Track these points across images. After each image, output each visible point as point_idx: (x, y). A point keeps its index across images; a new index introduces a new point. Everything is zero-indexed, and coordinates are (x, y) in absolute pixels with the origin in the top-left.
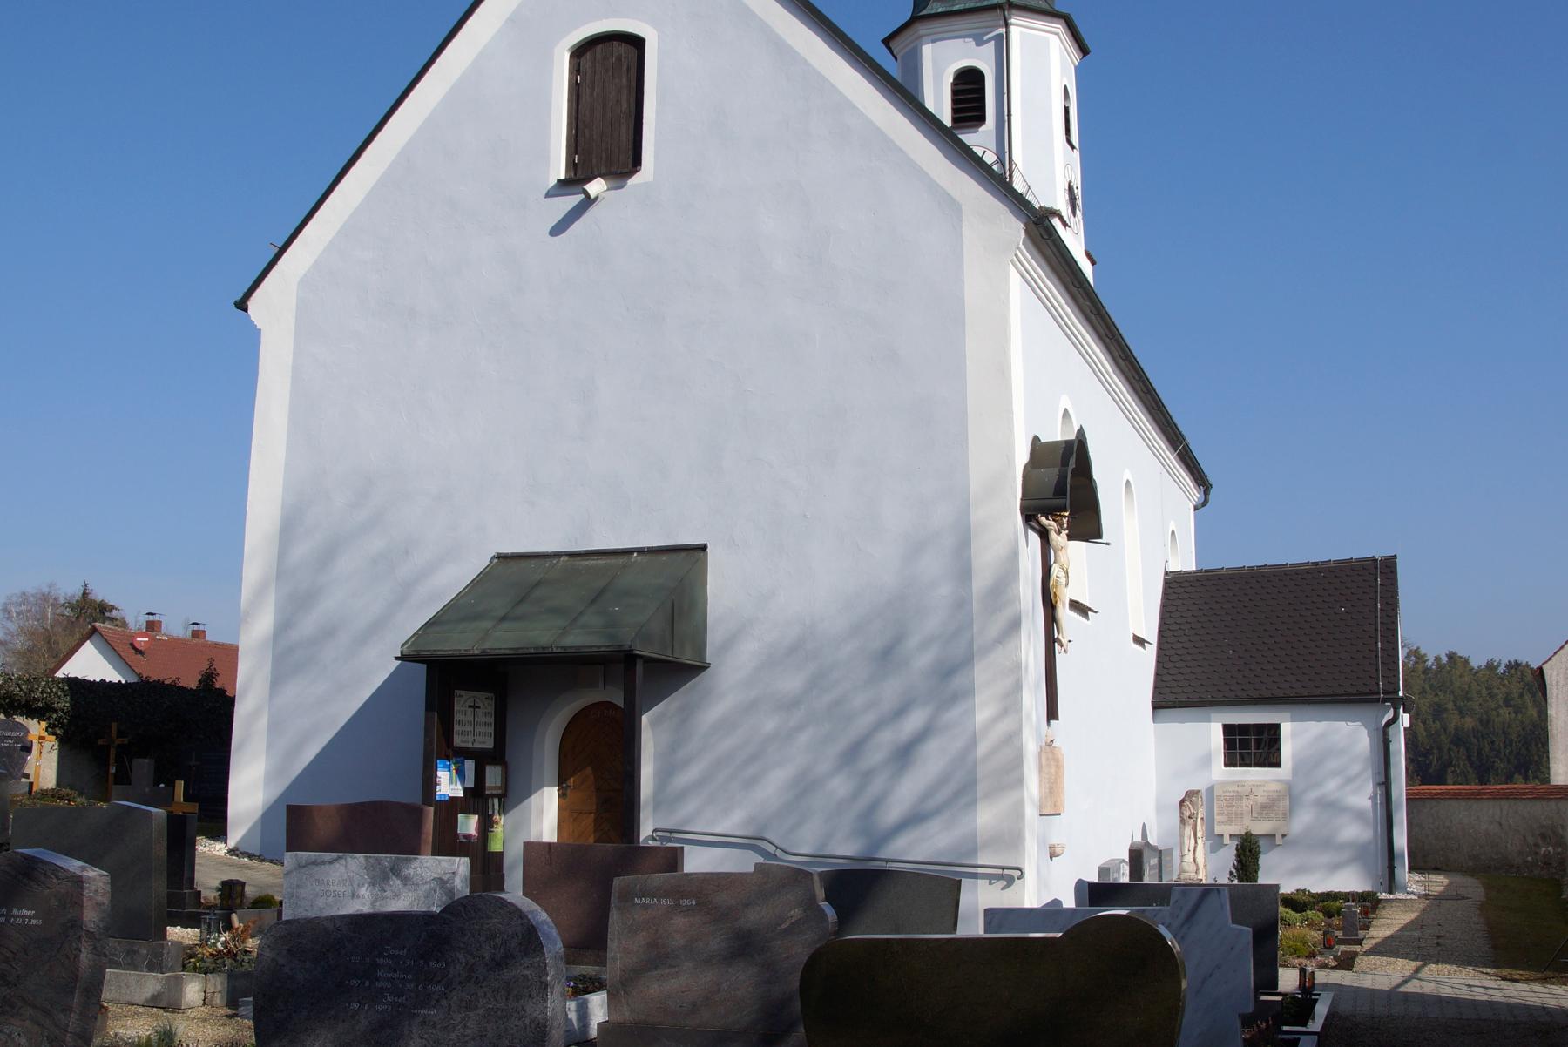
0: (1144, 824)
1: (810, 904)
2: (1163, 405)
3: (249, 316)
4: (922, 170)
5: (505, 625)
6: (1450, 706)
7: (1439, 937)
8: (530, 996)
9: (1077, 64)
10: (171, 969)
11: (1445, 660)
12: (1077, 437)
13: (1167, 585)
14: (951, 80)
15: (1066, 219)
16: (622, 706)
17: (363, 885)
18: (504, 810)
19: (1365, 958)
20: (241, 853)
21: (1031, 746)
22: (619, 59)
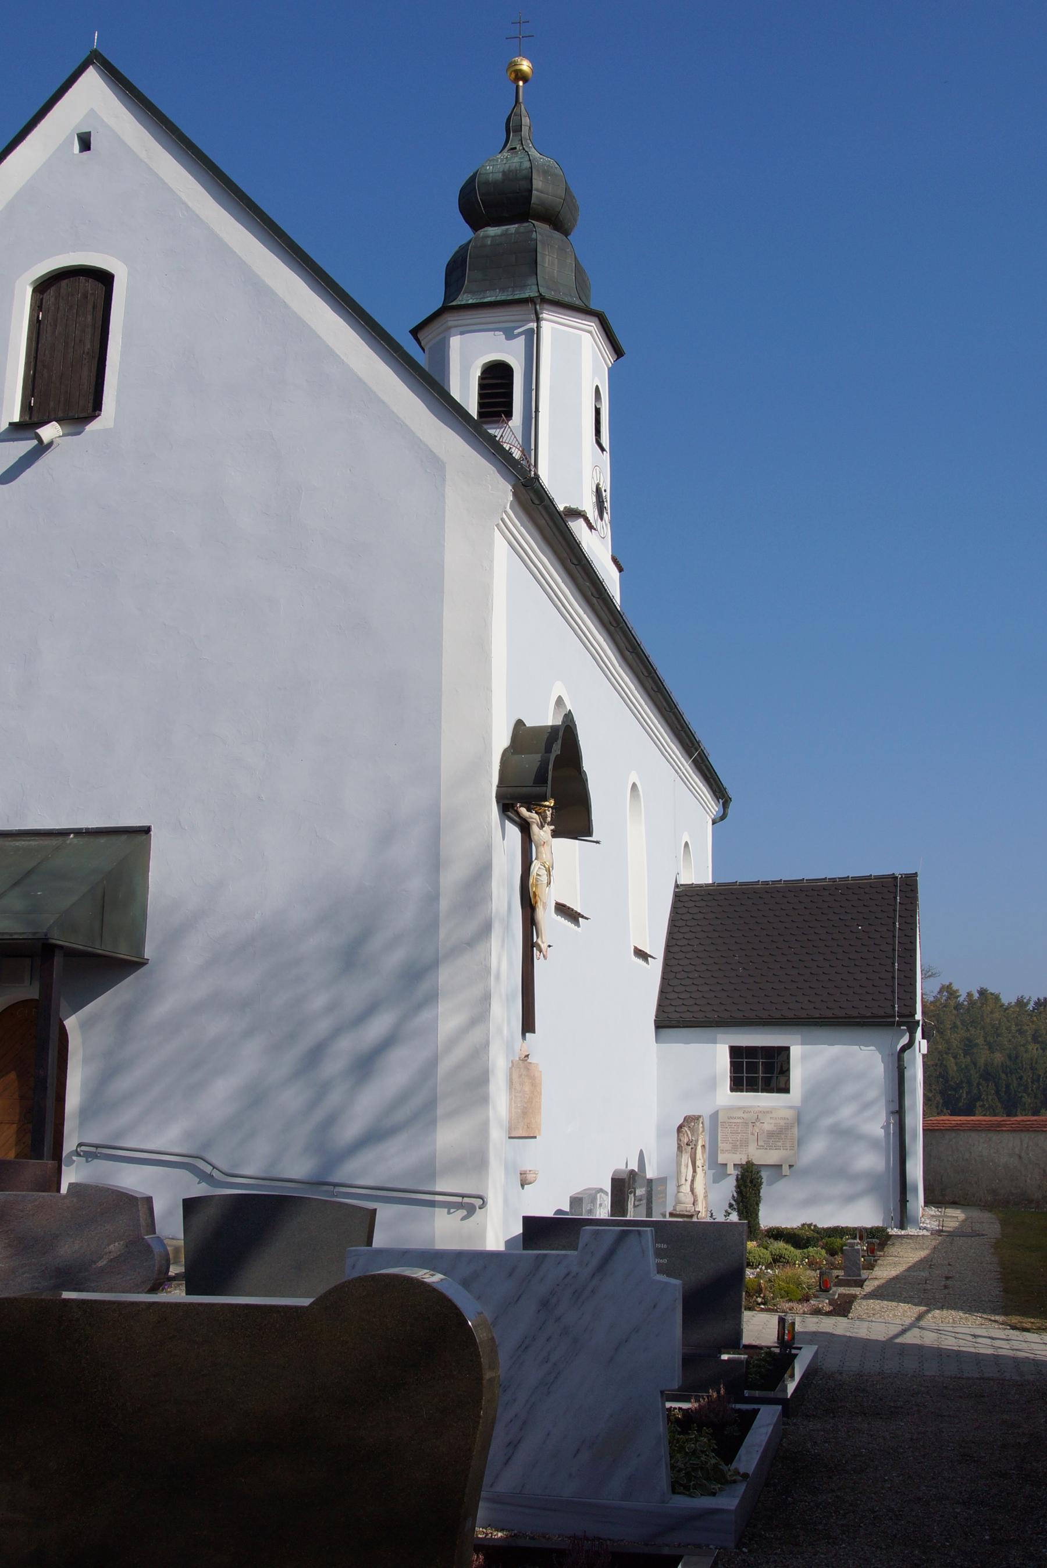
0: (641, 1151)
6: (980, 1041)
7: (947, 1278)
9: (610, 365)
11: (976, 996)
12: (563, 722)
13: (678, 898)
14: (479, 374)
19: (864, 1302)
21: (499, 1063)
22: (85, 296)
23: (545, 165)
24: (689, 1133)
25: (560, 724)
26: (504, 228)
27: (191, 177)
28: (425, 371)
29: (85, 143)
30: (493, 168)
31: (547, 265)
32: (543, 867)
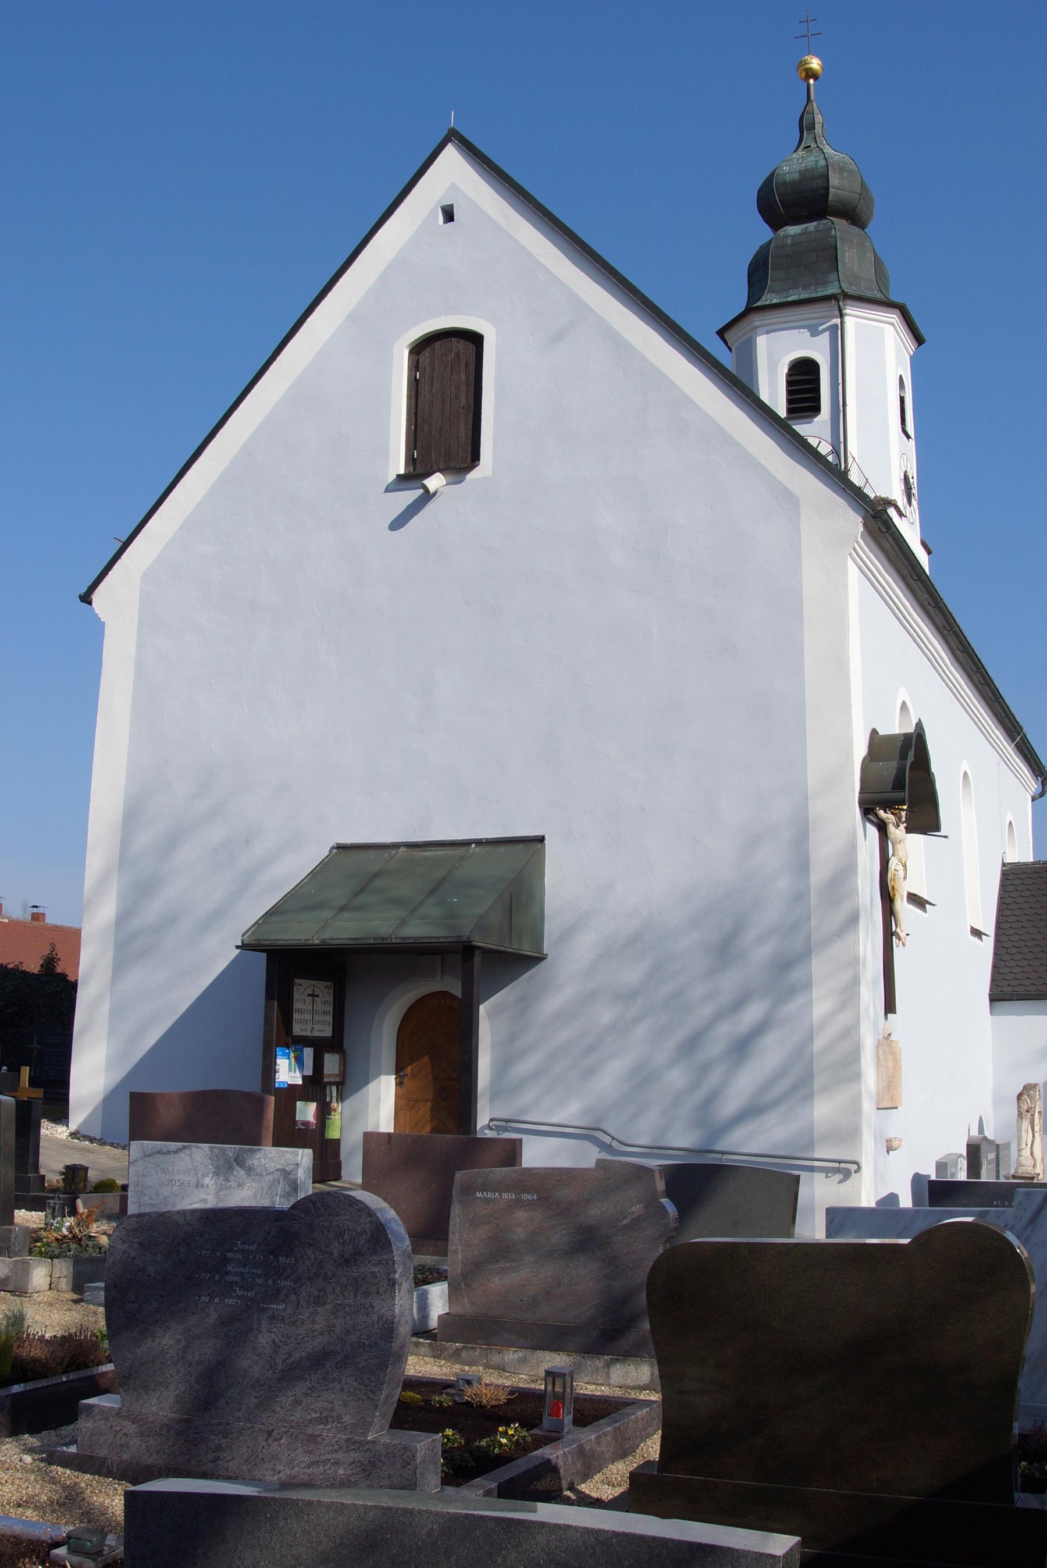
0: (981, 1118)
1: (651, 1202)
2: (1001, 696)
3: (94, 610)
4: (759, 463)
5: (345, 915)
8: (378, 1293)
9: (912, 353)
10: (17, 1254)
12: (915, 730)
14: (786, 371)
15: (902, 509)
16: (460, 996)
17: (207, 1175)
18: (341, 1098)
20: (82, 1136)
21: (868, 1041)
22: (458, 356)
23: (840, 161)
24: (1028, 1100)
25: (913, 731)
26: (804, 226)
27: (548, 242)
28: (733, 374)
29: (449, 215)
30: (789, 168)
31: (847, 261)
32: (899, 863)
